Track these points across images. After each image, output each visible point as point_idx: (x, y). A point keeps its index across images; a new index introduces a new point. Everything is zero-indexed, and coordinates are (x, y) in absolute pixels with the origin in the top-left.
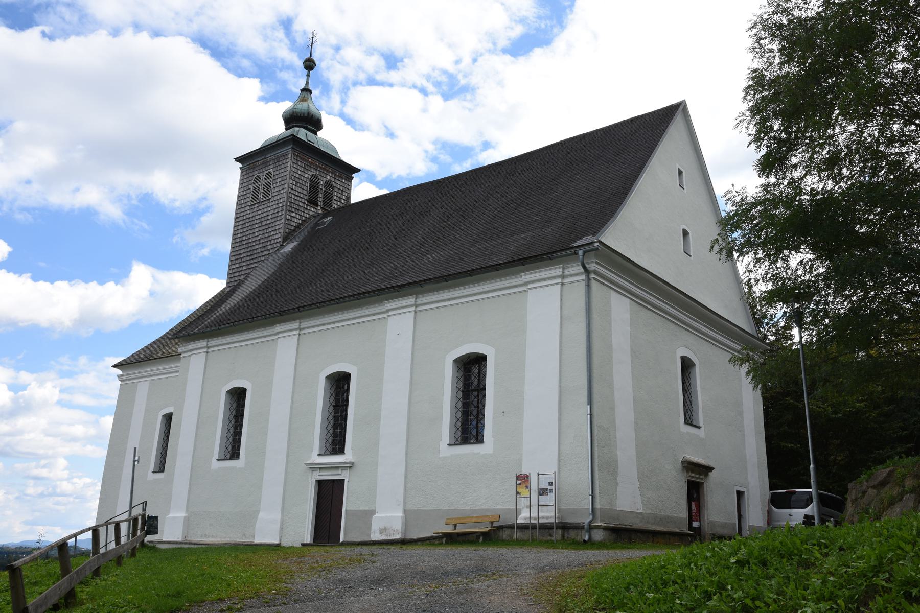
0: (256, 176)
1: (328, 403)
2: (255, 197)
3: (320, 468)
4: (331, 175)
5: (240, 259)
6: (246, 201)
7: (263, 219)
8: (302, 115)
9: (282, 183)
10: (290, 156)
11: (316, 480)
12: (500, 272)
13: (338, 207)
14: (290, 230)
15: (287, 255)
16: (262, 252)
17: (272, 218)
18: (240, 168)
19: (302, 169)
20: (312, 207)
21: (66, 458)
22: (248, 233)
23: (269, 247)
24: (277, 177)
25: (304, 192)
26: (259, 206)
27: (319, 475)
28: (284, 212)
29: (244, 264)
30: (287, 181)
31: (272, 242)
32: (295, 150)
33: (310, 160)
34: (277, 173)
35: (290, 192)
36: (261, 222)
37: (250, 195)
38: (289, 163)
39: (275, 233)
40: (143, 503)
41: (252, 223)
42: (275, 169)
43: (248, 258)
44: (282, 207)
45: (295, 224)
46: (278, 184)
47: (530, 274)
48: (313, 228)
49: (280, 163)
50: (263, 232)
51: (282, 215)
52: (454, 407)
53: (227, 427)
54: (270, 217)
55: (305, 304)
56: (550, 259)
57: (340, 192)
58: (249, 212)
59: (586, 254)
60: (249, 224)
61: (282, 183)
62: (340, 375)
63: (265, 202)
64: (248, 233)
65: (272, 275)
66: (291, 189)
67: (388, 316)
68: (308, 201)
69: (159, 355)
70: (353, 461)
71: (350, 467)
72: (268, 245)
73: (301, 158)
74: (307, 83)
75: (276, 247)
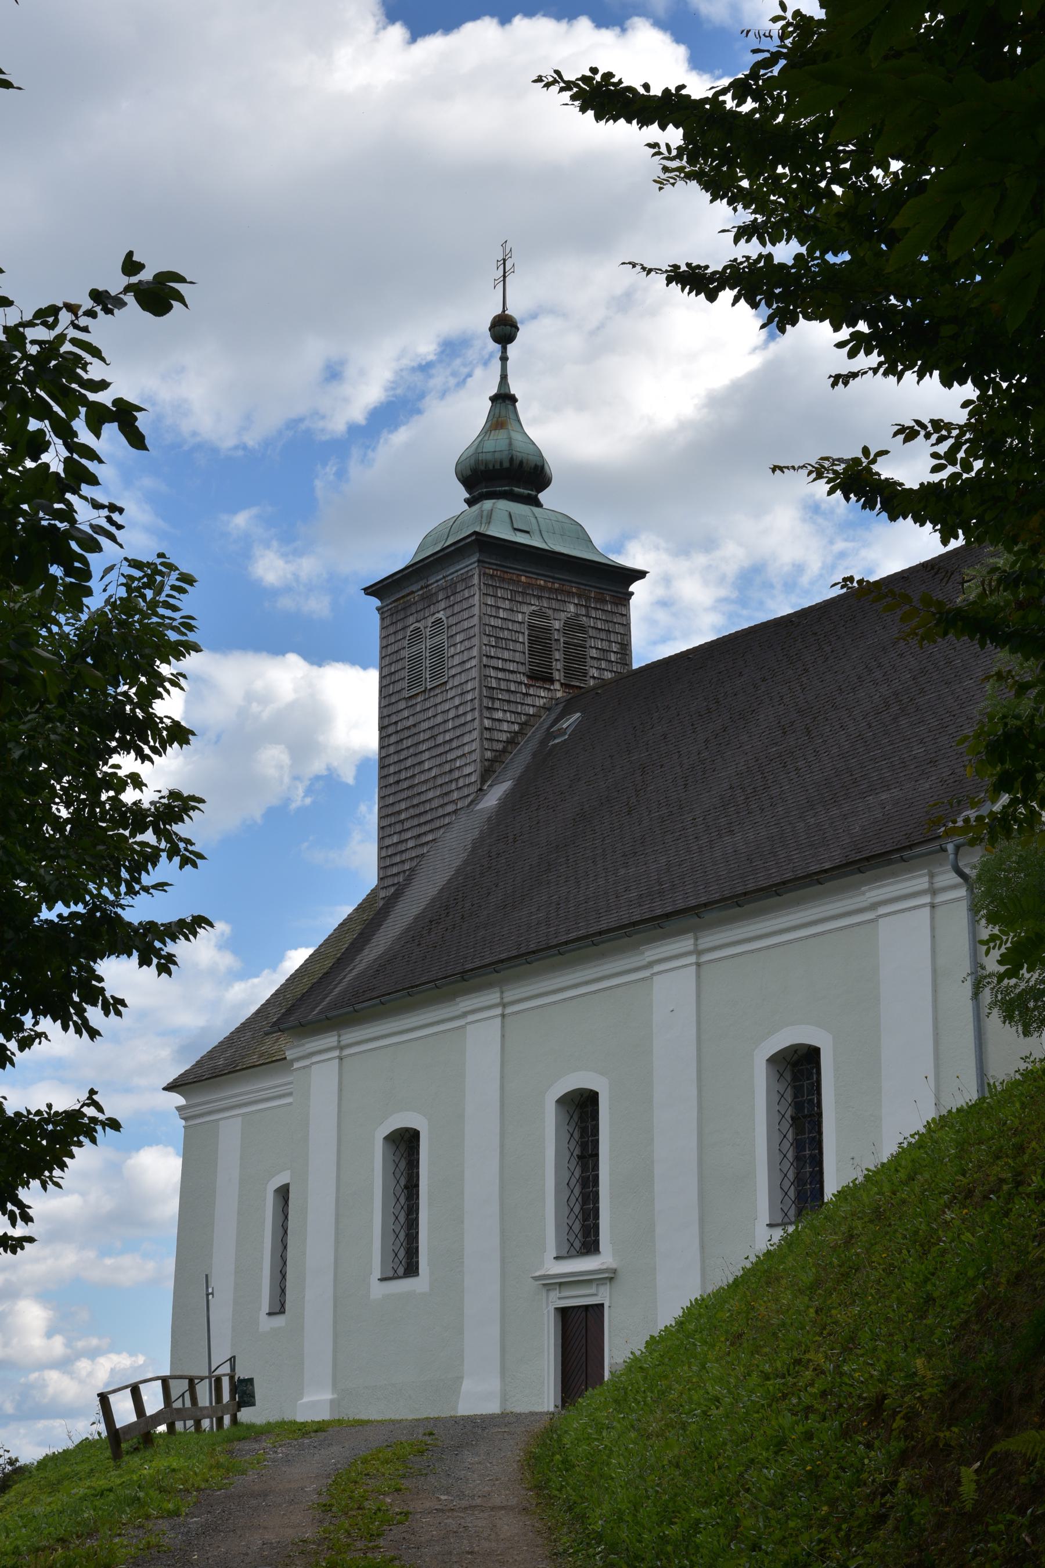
0: (411, 628)
1: (567, 1151)
2: (415, 679)
3: (561, 1284)
4: (576, 602)
5: (400, 824)
6: (398, 686)
7: (436, 731)
8: (498, 467)
9: (467, 644)
10: (476, 580)
11: (556, 1309)
12: (828, 885)
13: (597, 681)
14: (497, 751)
15: (489, 819)
16: (442, 806)
17: (454, 728)
18: (378, 609)
19: (507, 604)
20: (541, 687)
21: (43, 1297)
22: (409, 763)
23: (455, 795)
24: (454, 630)
25: (518, 657)
26: (425, 700)
27: (559, 1298)
28: (477, 714)
29: (409, 835)
30: (475, 641)
31: (461, 783)
32: (487, 566)
33: (523, 579)
34: (453, 620)
35: (485, 666)
36: (433, 737)
37: (404, 673)
38: (477, 597)
39: (463, 762)
40: (230, 1359)
41: (416, 739)
42: (449, 612)
43: (416, 822)
44: (472, 700)
45: (504, 737)
46: (459, 648)
47: (879, 887)
48: (543, 742)
49: (458, 598)
50: (438, 761)
51: (474, 720)
52: (776, 1154)
53: (392, 1210)
54: (450, 725)
55: (503, 956)
56: (903, 860)
57: (603, 635)
58: (406, 713)
59: (962, 849)
60: (409, 742)
61: (467, 644)
62: (582, 1096)
63: (438, 691)
64: (409, 763)
65: (459, 871)
66: (487, 656)
67: (653, 974)
68: (528, 677)
69: (254, 1059)
70: (614, 1266)
71: (611, 1279)
72: (452, 791)
73: (502, 580)
74: (504, 377)
75: (468, 795)
